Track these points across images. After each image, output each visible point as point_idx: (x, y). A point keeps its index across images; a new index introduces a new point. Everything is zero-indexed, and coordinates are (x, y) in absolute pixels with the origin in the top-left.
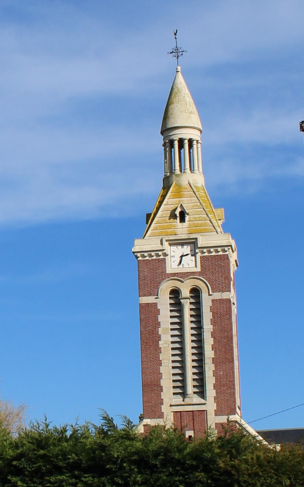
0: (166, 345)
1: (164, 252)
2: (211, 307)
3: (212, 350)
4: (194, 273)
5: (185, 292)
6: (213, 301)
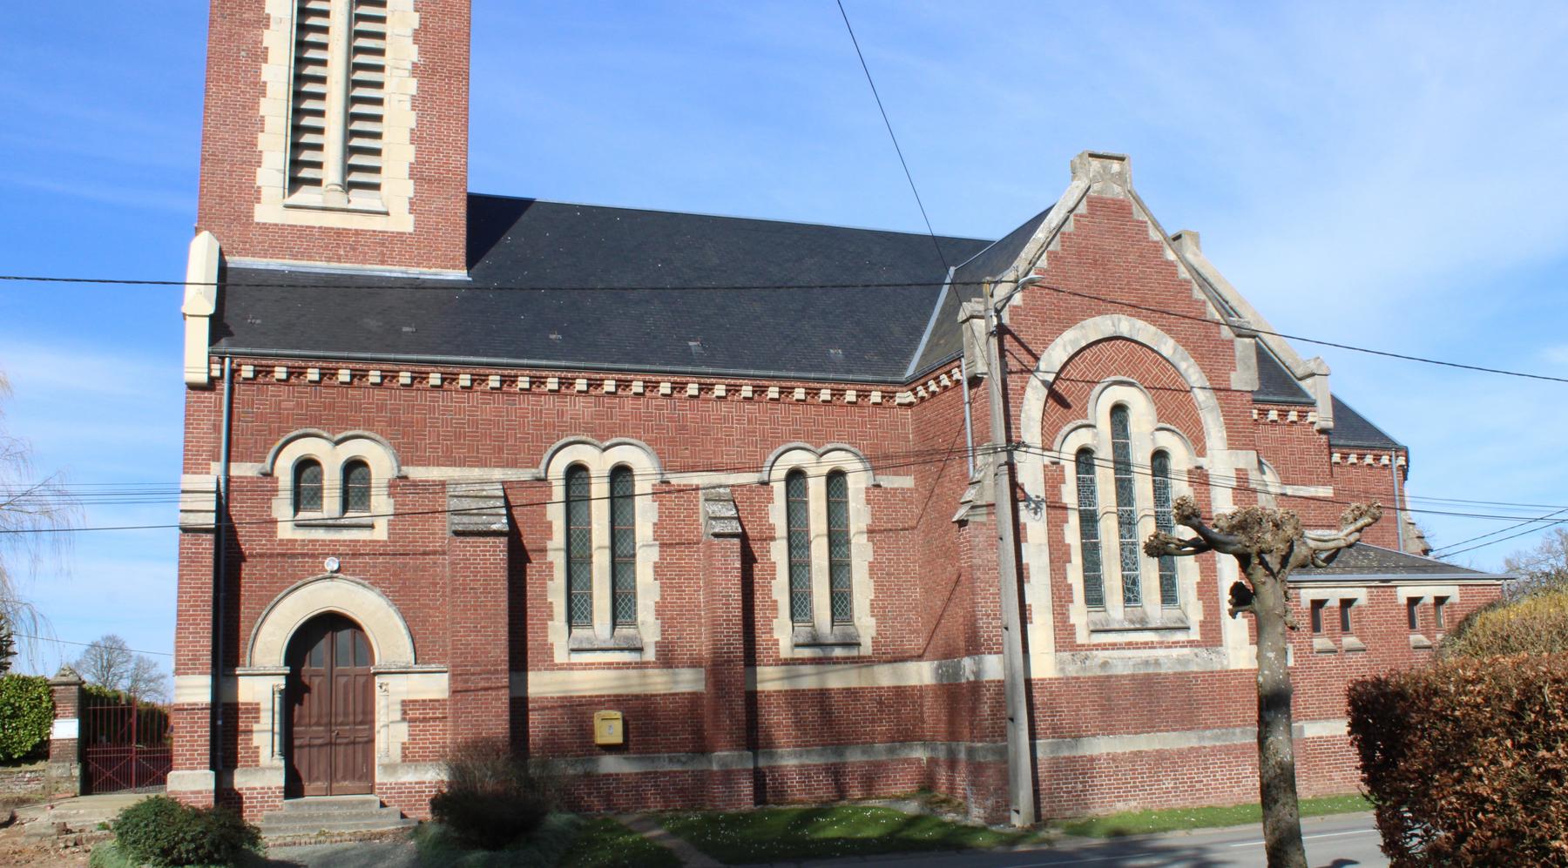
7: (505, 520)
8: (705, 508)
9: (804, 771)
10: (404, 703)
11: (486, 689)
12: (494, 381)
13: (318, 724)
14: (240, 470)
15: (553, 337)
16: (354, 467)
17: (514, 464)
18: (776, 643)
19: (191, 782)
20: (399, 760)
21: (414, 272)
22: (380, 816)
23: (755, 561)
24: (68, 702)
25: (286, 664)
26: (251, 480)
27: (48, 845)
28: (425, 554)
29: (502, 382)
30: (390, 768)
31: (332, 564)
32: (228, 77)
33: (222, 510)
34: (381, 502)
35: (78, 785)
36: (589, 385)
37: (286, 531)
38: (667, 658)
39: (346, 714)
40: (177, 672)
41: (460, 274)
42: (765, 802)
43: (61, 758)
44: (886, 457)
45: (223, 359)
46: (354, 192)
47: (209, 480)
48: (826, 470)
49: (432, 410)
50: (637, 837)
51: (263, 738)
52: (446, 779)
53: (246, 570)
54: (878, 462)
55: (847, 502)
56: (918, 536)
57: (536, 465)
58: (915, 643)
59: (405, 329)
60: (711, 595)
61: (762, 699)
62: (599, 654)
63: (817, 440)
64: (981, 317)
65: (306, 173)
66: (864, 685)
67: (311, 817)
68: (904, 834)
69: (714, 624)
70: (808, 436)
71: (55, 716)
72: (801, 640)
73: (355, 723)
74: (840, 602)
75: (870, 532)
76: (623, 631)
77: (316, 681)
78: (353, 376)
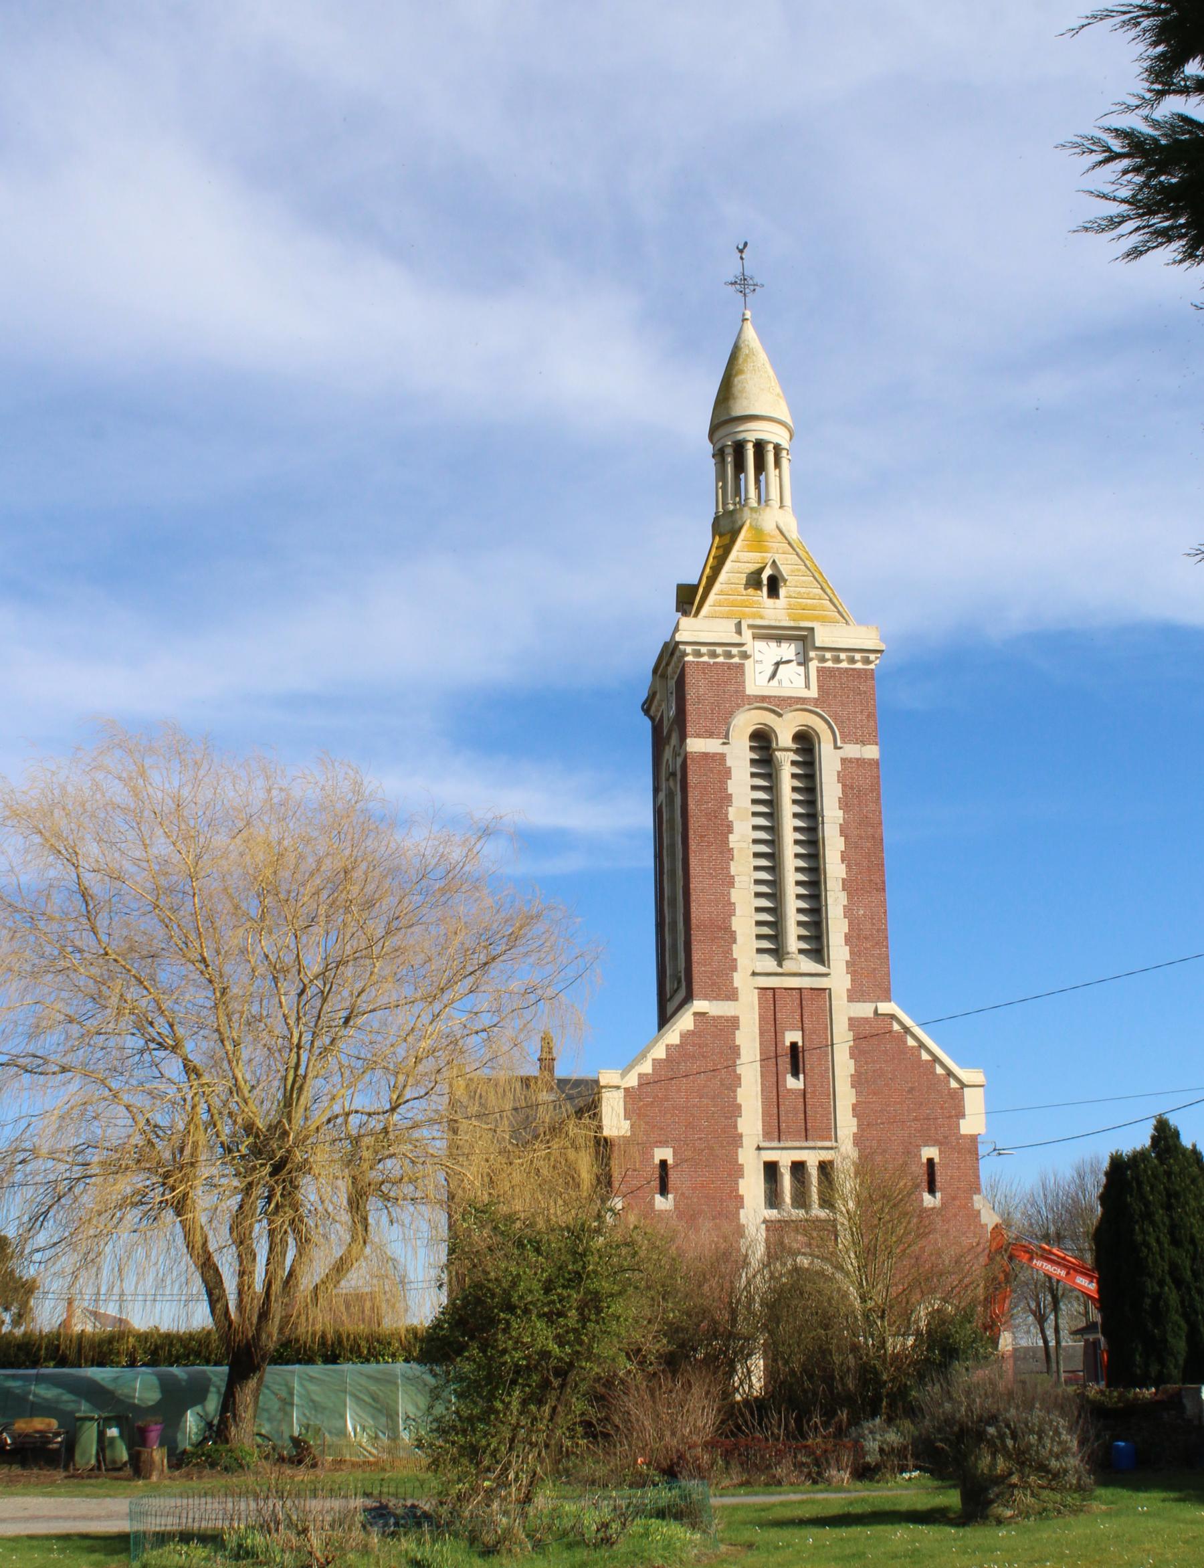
0: (744, 845)
1: (743, 649)
2: (839, 772)
3: (843, 861)
4: (803, 700)
5: (784, 737)
6: (843, 761)
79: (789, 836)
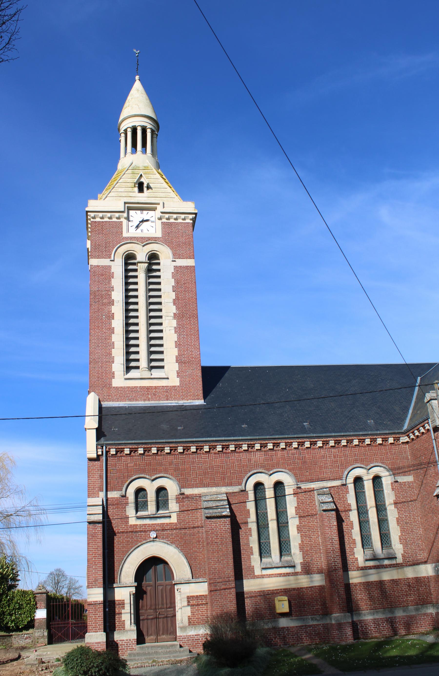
5: (141, 255)
6: (176, 267)
7: (228, 510)
8: (318, 498)
9: (375, 621)
10: (188, 598)
11: (225, 589)
12: (219, 448)
13: (150, 609)
14: (111, 495)
15: (243, 426)
16: (161, 490)
17: (230, 484)
18: (357, 559)
19: (95, 638)
20: (187, 624)
21: (181, 402)
22: (180, 652)
23: (343, 521)
24: (42, 603)
25: (135, 581)
26: (117, 499)
27: (34, 669)
28: (194, 528)
29: (223, 448)
30: (183, 628)
31: (153, 535)
32: (98, 327)
33: (105, 513)
34: (173, 506)
35: (46, 640)
36: (261, 447)
37: (133, 521)
38: (307, 570)
39: (163, 604)
40: (88, 587)
41: (201, 402)
42: (358, 638)
43: (39, 628)
44: (399, 468)
45: (102, 447)
46: (153, 370)
47: (98, 500)
48: (371, 477)
49: (193, 463)
50: (299, 658)
51: (126, 616)
52: (209, 633)
53: (116, 539)
54: (395, 471)
55: (383, 491)
56: (418, 504)
57: (240, 484)
58: (423, 556)
59: (179, 428)
60: (325, 539)
61: (353, 588)
62: (275, 570)
63: (366, 463)
64: (435, 399)
65: (133, 364)
66: (400, 577)
67: (149, 654)
68: (429, 653)
69: (327, 552)
70: (362, 461)
71: (37, 608)
72: (368, 558)
73: (167, 608)
74: (385, 538)
75: (395, 503)
76: (285, 558)
77: (149, 588)
78: (158, 451)
79: (142, 314)
